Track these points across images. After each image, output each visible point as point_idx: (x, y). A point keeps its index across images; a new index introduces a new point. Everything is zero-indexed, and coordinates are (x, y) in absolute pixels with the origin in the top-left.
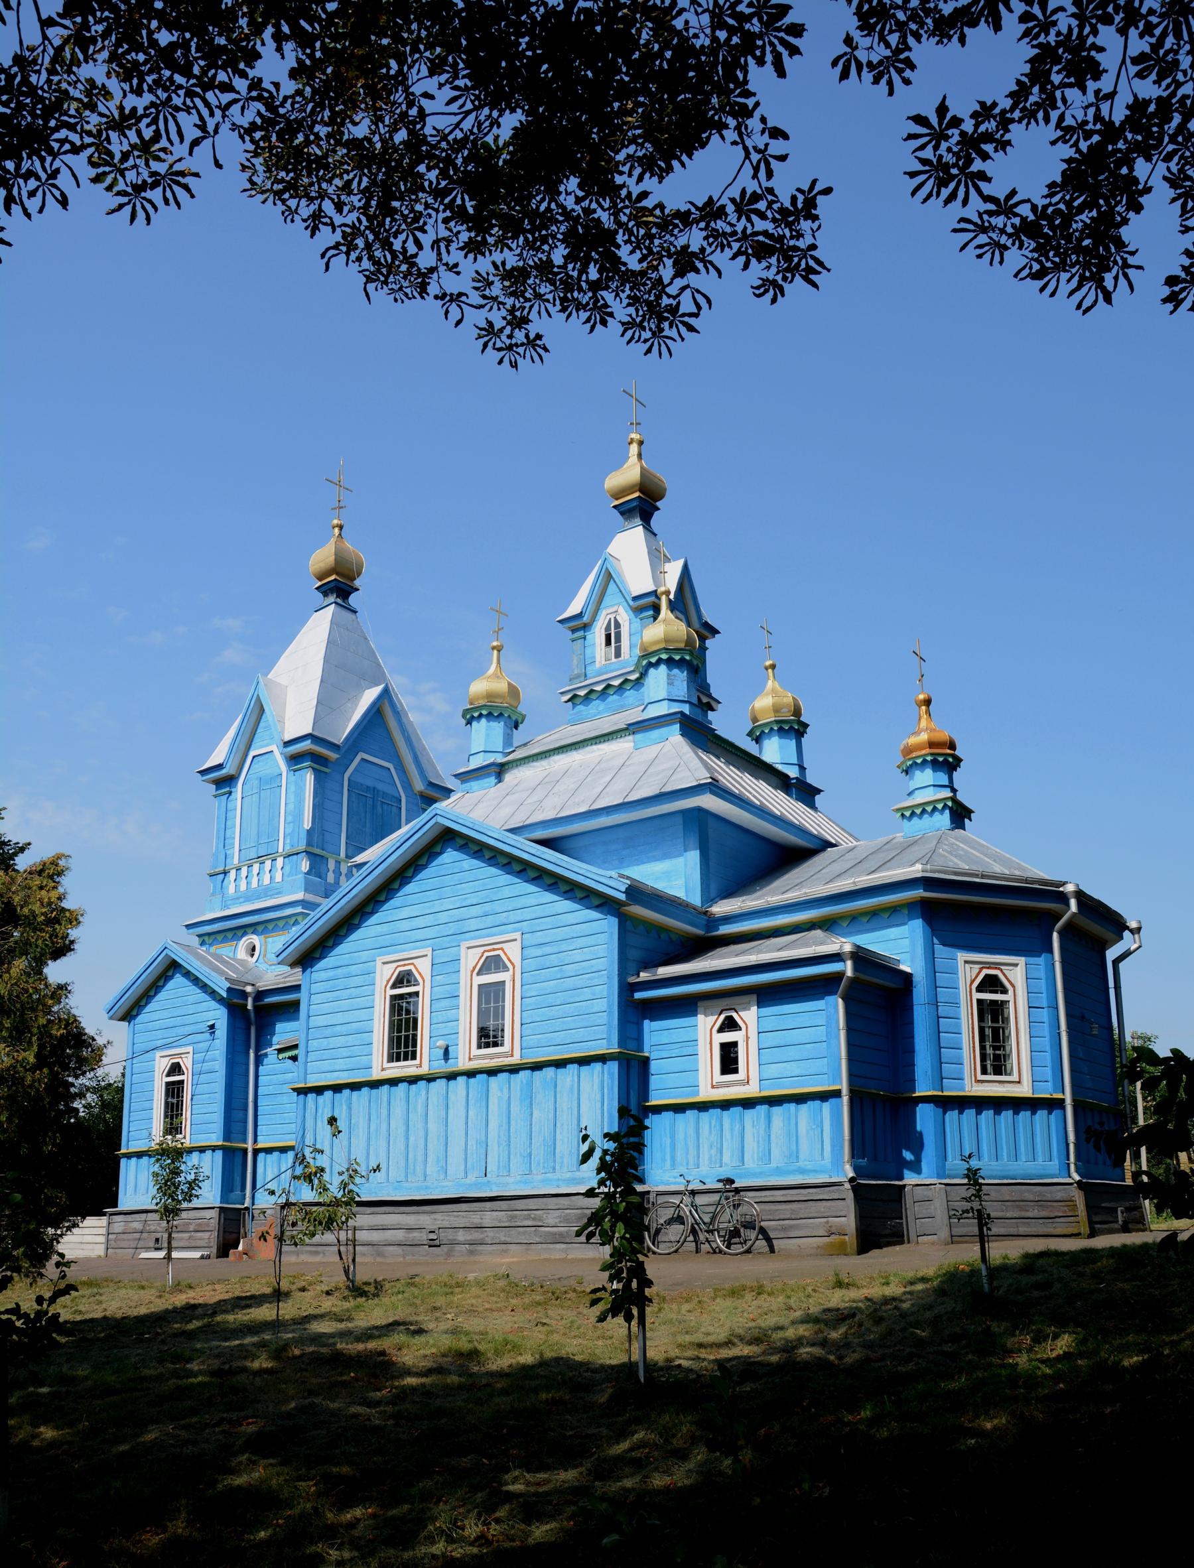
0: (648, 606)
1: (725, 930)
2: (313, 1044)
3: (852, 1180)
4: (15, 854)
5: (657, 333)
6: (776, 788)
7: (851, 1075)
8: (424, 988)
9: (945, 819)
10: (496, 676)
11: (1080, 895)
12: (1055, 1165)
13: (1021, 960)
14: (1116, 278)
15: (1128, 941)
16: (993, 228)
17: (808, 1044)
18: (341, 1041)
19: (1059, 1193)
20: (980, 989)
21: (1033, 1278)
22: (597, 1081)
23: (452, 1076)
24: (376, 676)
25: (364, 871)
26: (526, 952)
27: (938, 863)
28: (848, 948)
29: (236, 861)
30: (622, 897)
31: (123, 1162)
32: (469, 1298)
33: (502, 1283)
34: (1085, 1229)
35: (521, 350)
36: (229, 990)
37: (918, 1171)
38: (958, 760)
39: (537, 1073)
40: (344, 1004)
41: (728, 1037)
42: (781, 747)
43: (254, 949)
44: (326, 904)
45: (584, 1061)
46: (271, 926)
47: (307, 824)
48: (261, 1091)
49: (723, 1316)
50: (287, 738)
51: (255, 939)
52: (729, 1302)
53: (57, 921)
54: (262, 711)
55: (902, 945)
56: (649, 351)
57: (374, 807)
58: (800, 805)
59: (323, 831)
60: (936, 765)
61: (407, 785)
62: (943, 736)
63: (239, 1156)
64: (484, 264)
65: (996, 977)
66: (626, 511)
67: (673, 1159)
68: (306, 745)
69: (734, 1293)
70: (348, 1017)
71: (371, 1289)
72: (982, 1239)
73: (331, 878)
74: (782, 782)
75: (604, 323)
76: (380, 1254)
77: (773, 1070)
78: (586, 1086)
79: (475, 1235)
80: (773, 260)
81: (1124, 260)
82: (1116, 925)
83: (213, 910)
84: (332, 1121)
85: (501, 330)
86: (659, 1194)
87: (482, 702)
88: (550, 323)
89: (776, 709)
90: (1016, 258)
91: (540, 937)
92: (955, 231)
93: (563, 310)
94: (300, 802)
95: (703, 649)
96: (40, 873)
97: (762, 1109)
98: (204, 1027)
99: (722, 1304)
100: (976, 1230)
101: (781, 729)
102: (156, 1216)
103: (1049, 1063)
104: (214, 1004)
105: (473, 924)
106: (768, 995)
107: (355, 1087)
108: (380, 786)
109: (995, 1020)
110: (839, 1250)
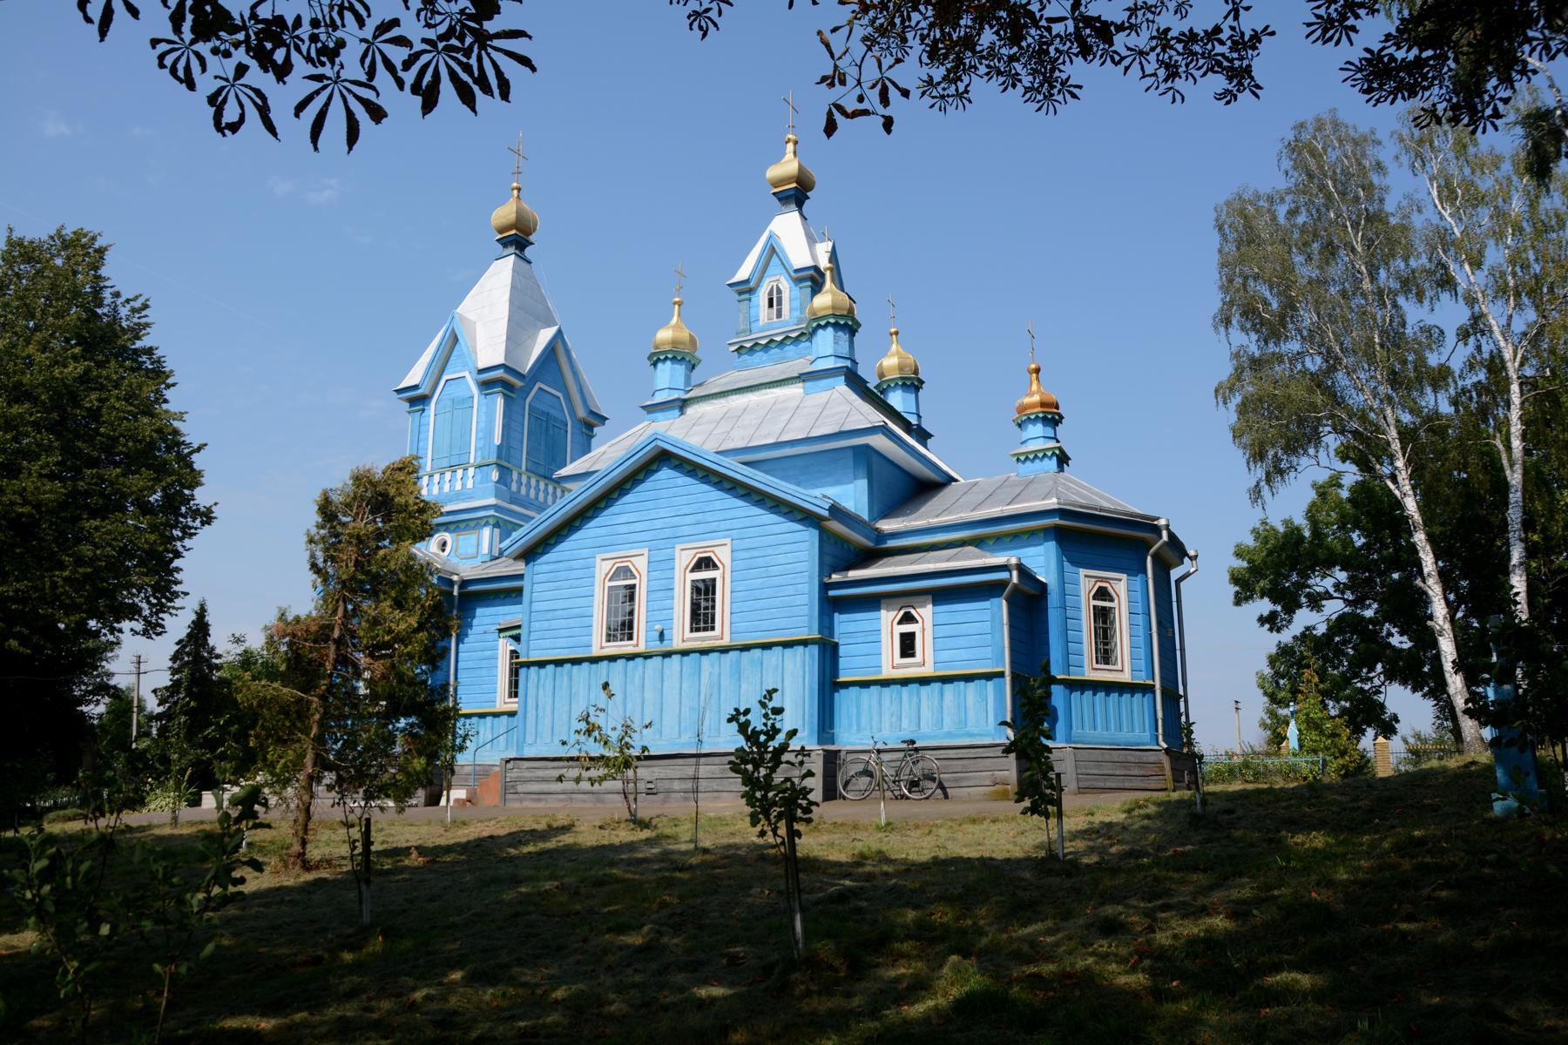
0: (813, 279)
1: (891, 543)
2: (535, 626)
4: (191, 453)
7: (1013, 662)
9: (1052, 464)
10: (676, 327)
13: (1124, 576)
17: (982, 634)
18: (563, 623)
19: (1152, 757)
22: (799, 659)
23: (667, 655)
24: (549, 322)
26: (737, 554)
28: (1014, 561)
29: (428, 469)
30: (826, 513)
34: (1170, 785)
38: (1061, 417)
40: (565, 593)
42: (904, 399)
43: (444, 544)
45: (787, 645)
46: (462, 526)
47: (497, 441)
48: (460, 665)
50: (481, 366)
51: (447, 536)
54: (456, 339)
55: (1042, 560)
59: (509, 448)
61: (572, 411)
62: (1054, 397)
67: (859, 725)
68: (499, 373)
70: (568, 604)
73: (514, 487)
75: (1014, 86)
76: (599, 801)
77: (945, 655)
84: (606, 686)
86: (848, 752)
87: (668, 348)
89: (901, 368)
91: (748, 543)
94: (491, 421)
96: (400, 469)
97: (936, 686)
99: (970, 828)
105: (686, 530)
106: (941, 596)
107: (576, 662)
108: (552, 412)
109: (1105, 622)
110: (1003, 796)
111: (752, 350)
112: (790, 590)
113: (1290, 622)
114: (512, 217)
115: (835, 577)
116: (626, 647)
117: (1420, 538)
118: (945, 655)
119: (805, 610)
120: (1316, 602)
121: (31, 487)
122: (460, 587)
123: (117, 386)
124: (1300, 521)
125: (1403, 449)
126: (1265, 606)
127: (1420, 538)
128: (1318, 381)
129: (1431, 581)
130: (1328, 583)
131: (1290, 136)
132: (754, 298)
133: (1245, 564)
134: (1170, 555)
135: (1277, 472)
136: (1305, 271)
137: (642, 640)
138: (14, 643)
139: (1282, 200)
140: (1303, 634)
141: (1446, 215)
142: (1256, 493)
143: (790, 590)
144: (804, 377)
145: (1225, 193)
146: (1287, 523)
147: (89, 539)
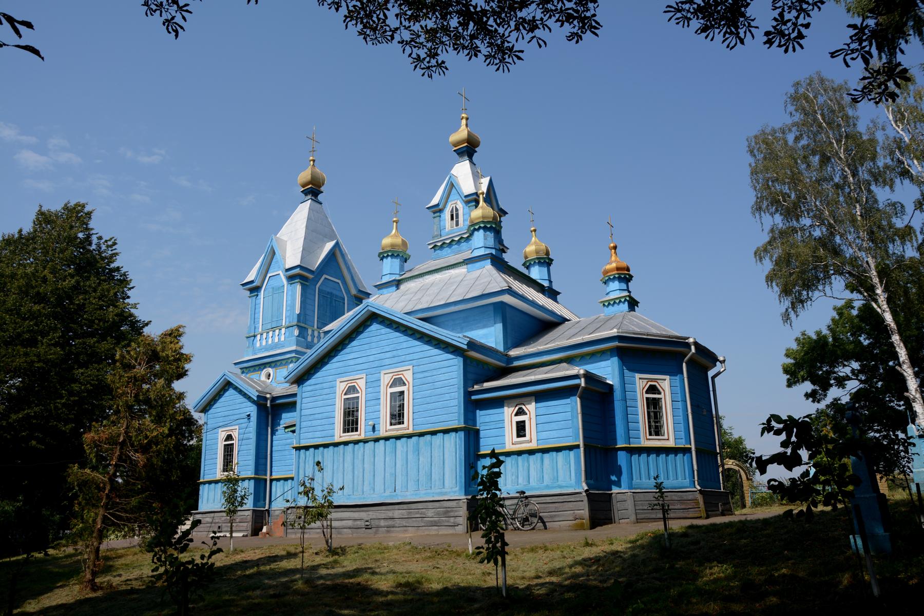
0: (473, 200)
1: (516, 364)
2: (304, 424)
3: (586, 491)
4: (143, 327)
5: (502, 60)
6: (538, 291)
7: (584, 437)
8: (362, 396)
9: (625, 306)
10: (395, 236)
11: (696, 344)
12: (687, 482)
13: (667, 377)
14: (745, 32)
15: (719, 367)
16: (684, 10)
17: (563, 421)
18: (319, 422)
19: (690, 496)
20: (647, 392)
21: (689, 539)
22: (453, 441)
23: (377, 440)
24: (332, 237)
25: (330, 335)
26: (416, 375)
27: (625, 328)
28: (582, 372)
30: (465, 347)
31: (201, 487)
32: (394, 554)
33: (408, 547)
34: (704, 514)
35: (434, 69)
36: (258, 396)
37: (620, 486)
38: (631, 277)
39: (421, 438)
41: (520, 418)
42: (540, 271)
43: (269, 375)
44: (309, 352)
46: (278, 363)
47: (297, 311)
48: (274, 449)
49: (530, 562)
50: (287, 267)
51: (270, 370)
52: (531, 555)
53: (179, 359)
54: (274, 253)
55: (608, 370)
56: (498, 69)
57: (331, 302)
58: (550, 300)
59: (305, 315)
60: (620, 279)
62: (624, 264)
63: (262, 484)
64: (416, 27)
65: (655, 386)
66: (460, 153)
68: (297, 271)
69: (533, 550)
71: (339, 551)
72: (665, 519)
73: (309, 339)
74: (540, 288)
75: (476, 56)
77: (544, 435)
78: (447, 444)
79: (390, 523)
80: (575, 22)
81: (749, 24)
82: (713, 359)
83: (248, 355)
84: (318, 463)
85: (424, 59)
87: (388, 249)
88: (448, 55)
89: (537, 252)
90: (696, 24)
92: (665, 12)
93: (456, 49)
94: (294, 300)
95: (500, 222)
96: (170, 335)
97: (539, 455)
98: (244, 415)
99: (527, 556)
100: (661, 516)
101: (539, 262)
102: (224, 514)
103: (683, 429)
104: (249, 404)
105: (387, 362)
106: (540, 397)
107: (326, 446)
108: (334, 292)
110: (581, 527)
111: (442, 247)
112: (447, 397)
113: (825, 395)
114: (309, 177)
115: (476, 387)
116: (353, 436)
117: (896, 338)
118: (544, 435)
119: (456, 409)
120: (841, 382)
121: (42, 351)
122: (271, 401)
123: (95, 291)
124: (825, 332)
125: (881, 282)
126: (808, 386)
127: (896, 338)
128: (825, 243)
129: (905, 367)
130: (847, 370)
131: (792, 91)
132: (442, 215)
133: (792, 361)
134: (704, 361)
135: (798, 302)
136: (809, 177)
137: (362, 433)
138: (34, 443)
139: (790, 130)
140: (832, 403)
141: (899, 130)
142: (786, 317)
143: (447, 397)
144: (467, 262)
145: (754, 131)
146: (818, 333)
147: (75, 381)
